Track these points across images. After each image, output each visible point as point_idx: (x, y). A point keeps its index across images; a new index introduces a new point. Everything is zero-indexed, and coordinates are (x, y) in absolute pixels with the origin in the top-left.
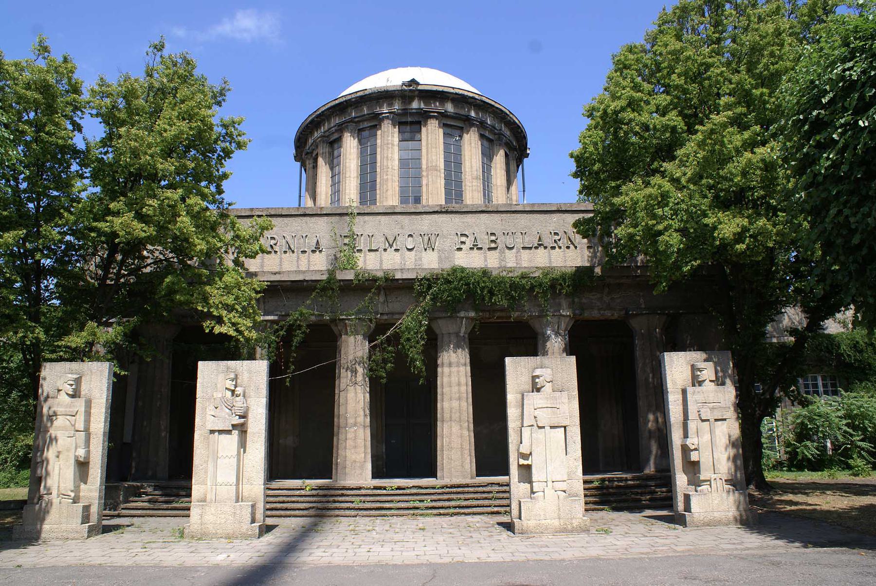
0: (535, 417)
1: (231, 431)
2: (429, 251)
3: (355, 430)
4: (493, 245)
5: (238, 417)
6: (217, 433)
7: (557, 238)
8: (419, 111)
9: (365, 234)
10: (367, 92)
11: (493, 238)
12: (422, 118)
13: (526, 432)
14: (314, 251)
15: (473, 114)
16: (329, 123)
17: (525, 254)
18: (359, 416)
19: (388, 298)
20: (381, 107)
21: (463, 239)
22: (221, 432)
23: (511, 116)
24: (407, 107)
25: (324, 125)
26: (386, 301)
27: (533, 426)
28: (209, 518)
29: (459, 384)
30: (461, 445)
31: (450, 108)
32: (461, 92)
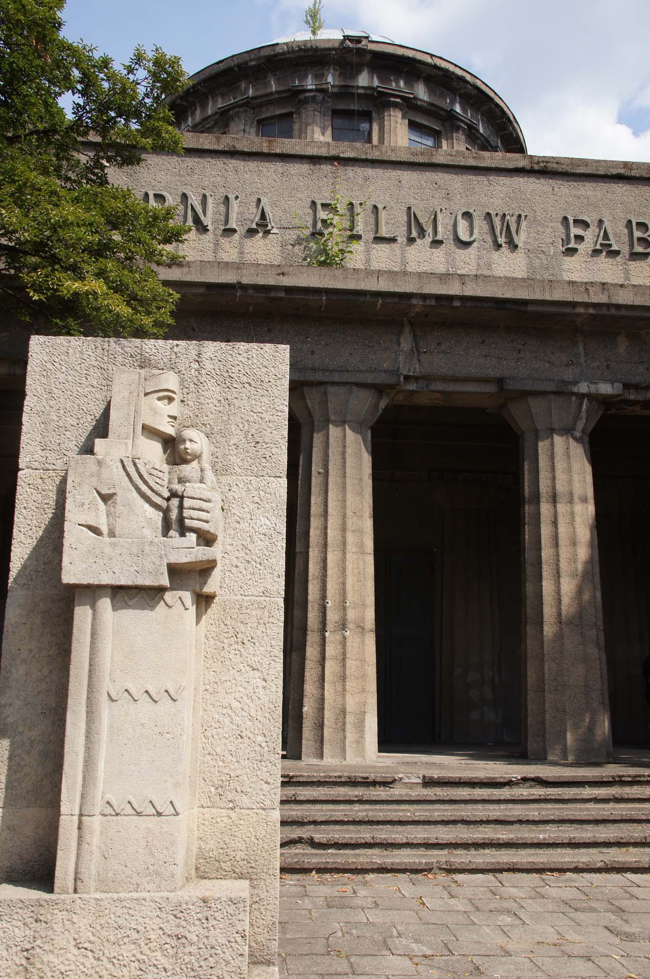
1: (161, 590)
8: (369, 92)
14: (251, 232)
15: (458, 109)
16: (204, 107)
20: (304, 77)
23: (515, 125)
24: (349, 83)
25: (193, 114)
26: (416, 351)
31: (421, 92)
32: (444, 65)
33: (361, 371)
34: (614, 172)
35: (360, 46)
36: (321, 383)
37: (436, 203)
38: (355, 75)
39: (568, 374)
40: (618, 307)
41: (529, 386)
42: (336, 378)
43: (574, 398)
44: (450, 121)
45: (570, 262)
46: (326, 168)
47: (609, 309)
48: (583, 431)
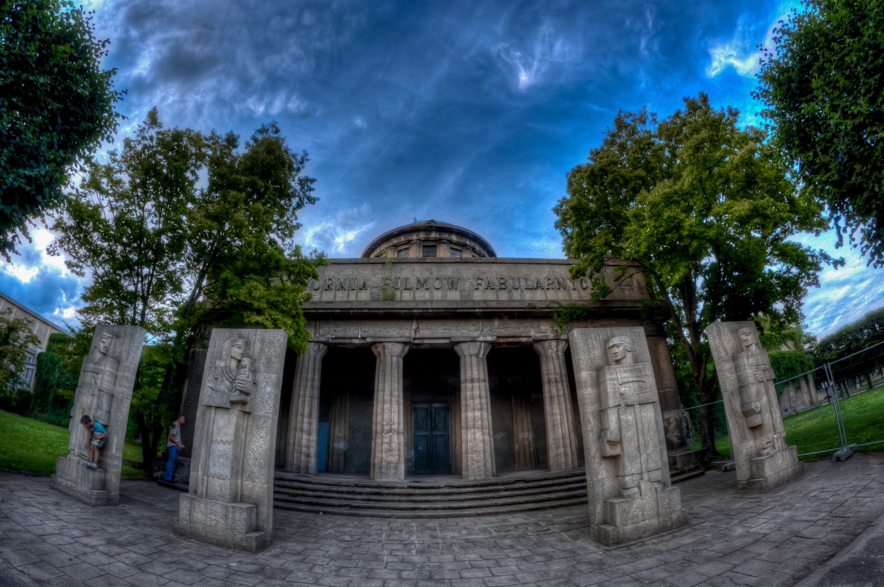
3: (391, 436)
4: (503, 286)
5: (237, 392)
6: (213, 409)
9: (402, 277)
11: (503, 281)
12: (439, 241)
13: (612, 420)
18: (394, 424)
21: (480, 281)
22: (217, 408)
27: (619, 405)
28: (199, 516)
29: (480, 397)
30: (484, 448)
36: (381, 342)
39: (476, 334)
44: (465, 246)
47: (432, 303)
48: (483, 355)
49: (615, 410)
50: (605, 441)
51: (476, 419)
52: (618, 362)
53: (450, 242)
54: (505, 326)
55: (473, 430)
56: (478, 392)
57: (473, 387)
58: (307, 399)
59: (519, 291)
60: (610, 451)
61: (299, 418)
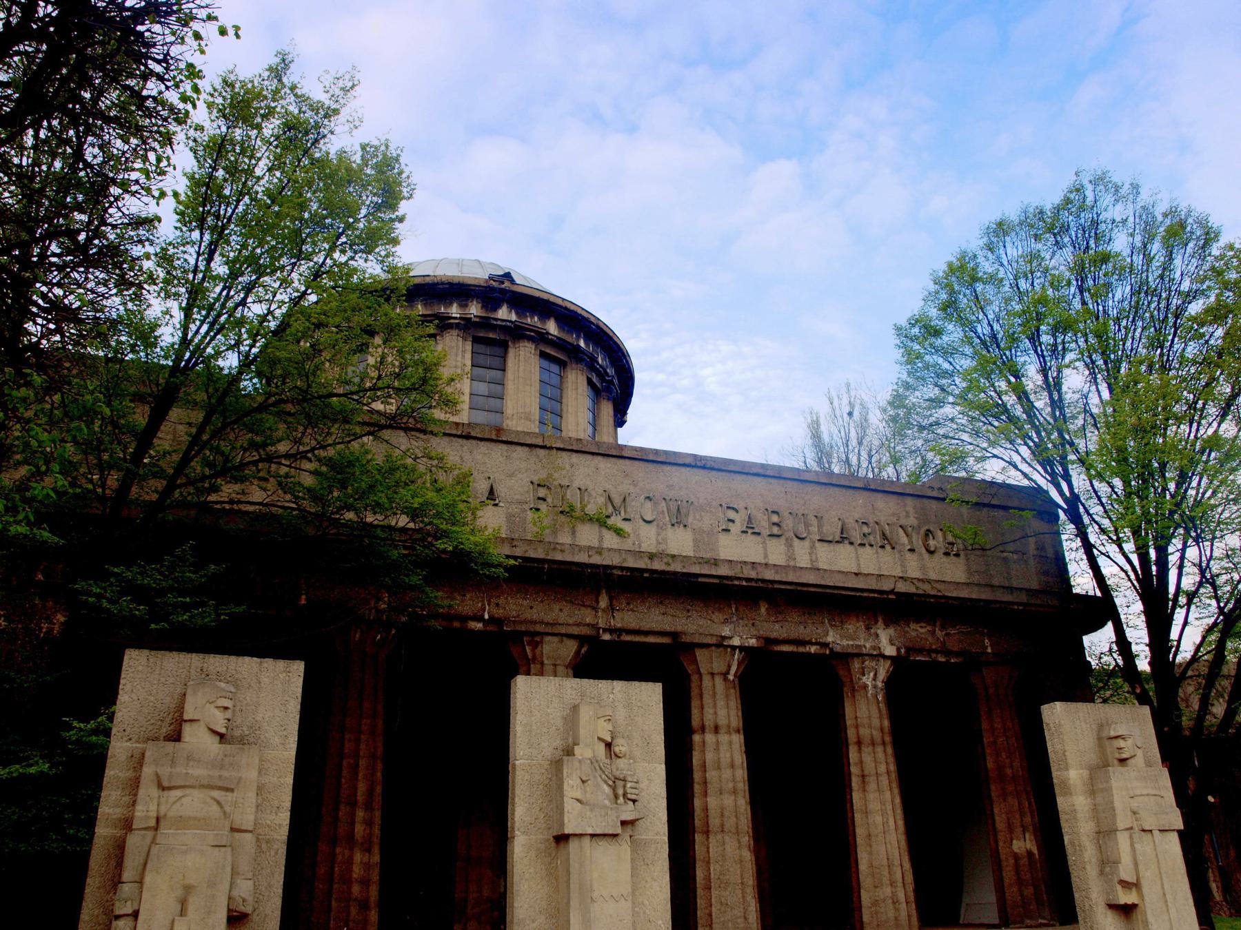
0: (1134, 813)
2: (680, 531)
4: (775, 530)
7: (866, 530)
10: (428, 280)
11: (775, 518)
12: (517, 333)
15: (582, 344)
17: (822, 550)
19: (615, 602)
21: (732, 515)
26: (611, 608)
27: (1131, 828)
29: (732, 766)
31: (552, 327)
32: (573, 308)
33: (568, 625)
34: (755, 471)
35: (503, 286)
37: (625, 487)
38: (495, 308)
39: (726, 631)
40: (764, 581)
41: (697, 640)
42: (549, 630)
43: (729, 650)
45: (724, 540)
46: (542, 452)
49: (1126, 835)
50: (1116, 880)
51: (726, 814)
52: (1123, 761)
53: (541, 338)
54: (780, 618)
55: (719, 837)
56: (728, 755)
57: (718, 742)
58: (363, 763)
59: (807, 543)
60: (1126, 898)
61: (343, 811)
